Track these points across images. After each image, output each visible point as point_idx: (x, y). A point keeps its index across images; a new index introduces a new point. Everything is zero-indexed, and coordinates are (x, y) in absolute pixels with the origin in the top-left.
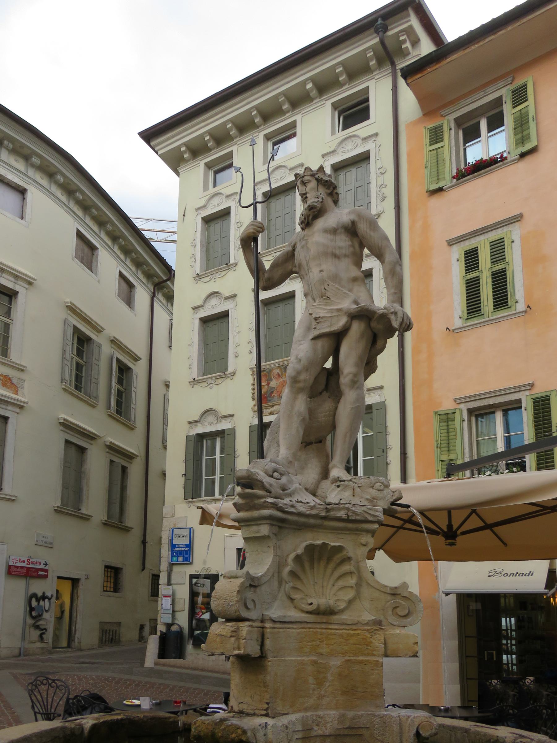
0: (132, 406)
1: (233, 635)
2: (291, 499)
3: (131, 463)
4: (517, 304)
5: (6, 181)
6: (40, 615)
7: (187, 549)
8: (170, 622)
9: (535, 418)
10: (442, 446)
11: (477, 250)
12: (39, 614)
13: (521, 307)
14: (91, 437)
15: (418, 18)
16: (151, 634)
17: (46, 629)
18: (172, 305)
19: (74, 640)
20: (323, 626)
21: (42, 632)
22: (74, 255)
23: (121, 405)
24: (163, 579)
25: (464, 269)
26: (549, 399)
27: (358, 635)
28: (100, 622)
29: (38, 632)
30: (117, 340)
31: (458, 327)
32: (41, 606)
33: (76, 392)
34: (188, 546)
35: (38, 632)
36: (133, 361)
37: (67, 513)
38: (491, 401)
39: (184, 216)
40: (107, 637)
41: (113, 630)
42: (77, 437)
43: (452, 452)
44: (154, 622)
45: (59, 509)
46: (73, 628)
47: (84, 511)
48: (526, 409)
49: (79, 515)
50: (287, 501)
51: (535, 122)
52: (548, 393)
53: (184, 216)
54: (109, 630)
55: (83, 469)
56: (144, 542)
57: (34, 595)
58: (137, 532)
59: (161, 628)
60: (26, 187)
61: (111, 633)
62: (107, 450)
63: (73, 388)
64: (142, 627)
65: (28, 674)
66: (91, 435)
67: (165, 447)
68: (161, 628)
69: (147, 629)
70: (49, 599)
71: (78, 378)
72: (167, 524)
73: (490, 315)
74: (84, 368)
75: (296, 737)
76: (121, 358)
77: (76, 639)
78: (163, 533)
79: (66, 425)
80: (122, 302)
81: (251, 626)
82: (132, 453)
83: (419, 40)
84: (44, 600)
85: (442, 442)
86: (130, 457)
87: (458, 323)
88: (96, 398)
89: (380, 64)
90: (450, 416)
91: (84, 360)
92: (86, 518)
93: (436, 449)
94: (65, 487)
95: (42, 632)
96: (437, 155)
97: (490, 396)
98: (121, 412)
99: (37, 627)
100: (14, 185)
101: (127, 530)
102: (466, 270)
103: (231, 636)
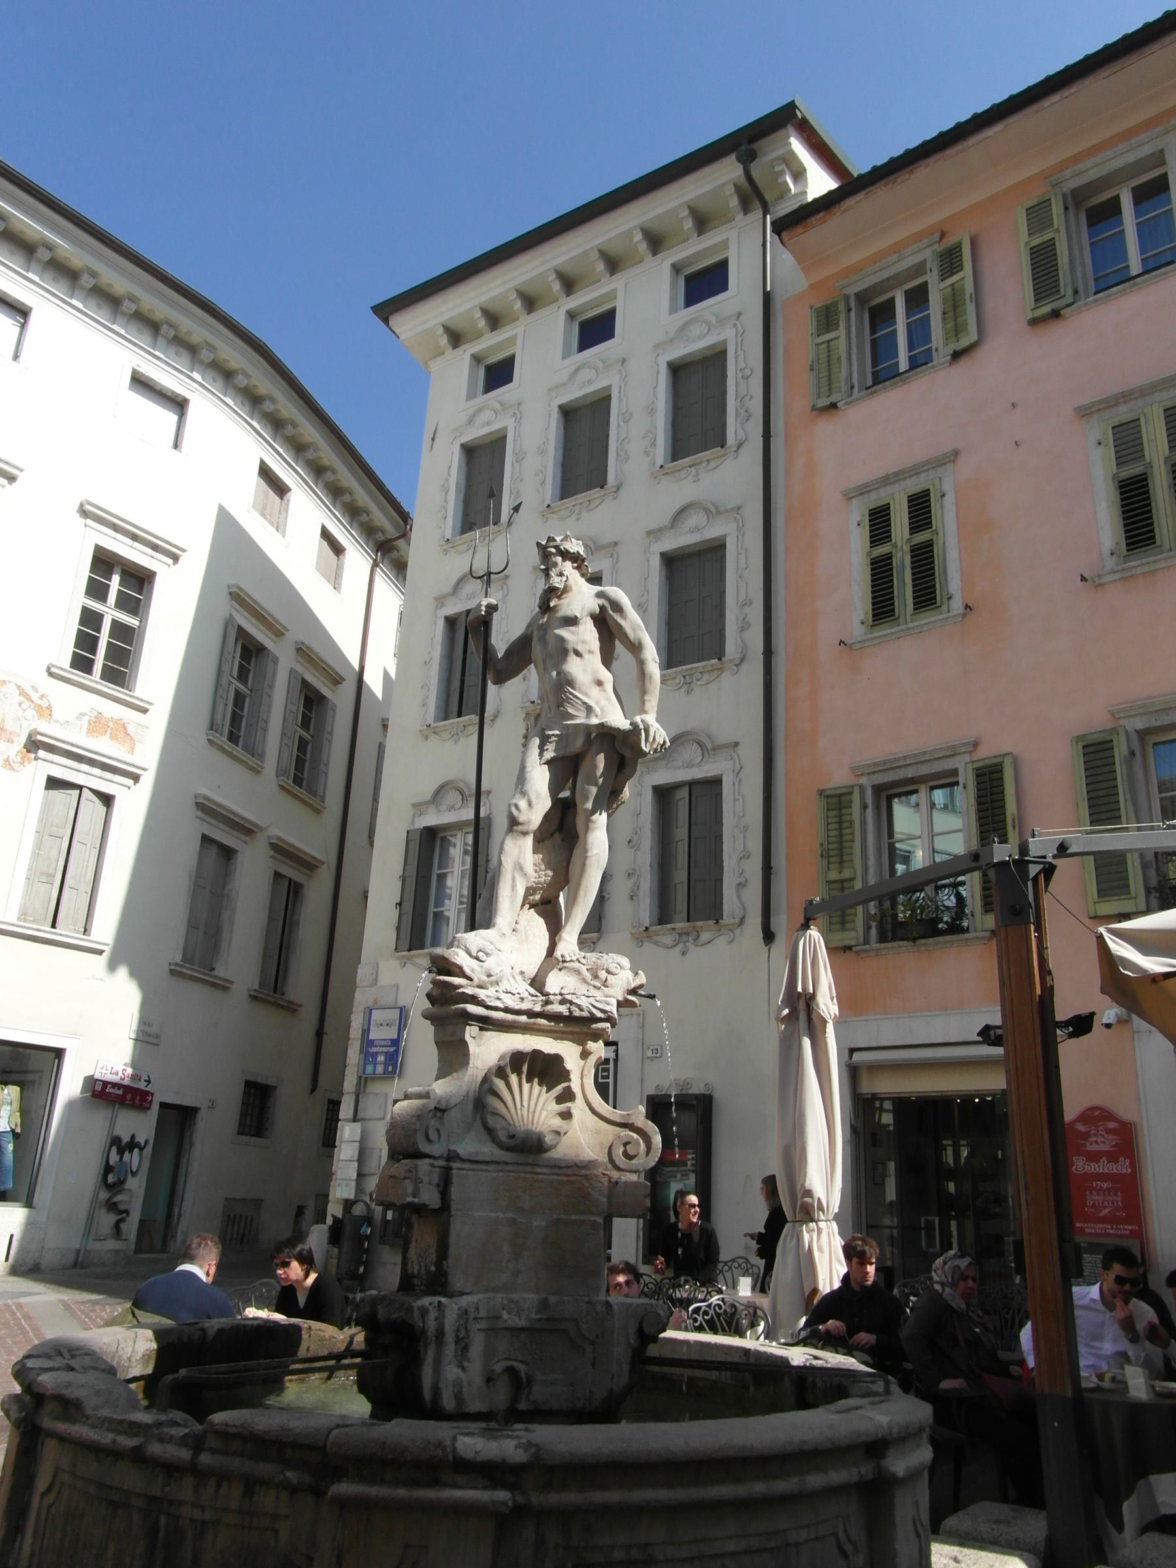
0: (322, 767)
1: (407, 1175)
2: (498, 988)
3: (310, 877)
4: (952, 601)
5: (158, 388)
6: (121, 1182)
7: (392, 1049)
8: (352, 1197)
9: (979, 804)
10: (832, 853)
11: (889, 509)
12: (119, 1179)
13: (957, 605)
14: (246, 829)
15: (802, 137)
16: (317, 1223)
17: (127, 1212)
18: (405, 578)
19: (174, 1237)
20: (528, 1169)
21: (120, 1217)
22: (251, 504)
23: (306, 747)
24: (346, 1111)
25: (868, 540)
26: (1001, 771)
27: (572, 1182)
28: (226, 1199)
29: (113, 1218)
30: (308, 648)
31: (859, 639)
32: (125, 1164)
33: (229, 746)
34: (396, 1043)
35: (113, 1218)
36: (329, 685)
37: (191, 976)
38: (910, 773)
39: (433, 439)
40: (236, 1230)
41: (247, 1217)
42: (223, 831)
43: (845, 865)
44: (323, 1198)
45: (178, 969)
46: (176, 1210)
47: (220, 971)
48: (965, 787)
49: (211, 980)
50: (491, 992)
51: (974, 303)
52: (999, 760)
53: (433, 439)
54: (241, 1217)
55: (226, 892)
56: (320, 1034)
57: (116, 1141)
58: (309, 1014)
59: (334, 1210)
60: (187, 397)
61: (243, 1223)
62: (272, 853)
63: (225, 739)
64: (300, 1211)
65: (89, 1301)
66: (246, 825)
67: (372, 844)
68: (334, 1210)
69: (309, 1214)
70: (141, 1149)
71: (236, 719)
72: (362, 998)
73: (909, 619)
74: (247, 701)
75: (478, 1326)
76: (310, 678)
77: (179, 1233)
78: (353, 1017)
79: (206, 808)
80: (322, 578)
81: (432, 1165)
82: (313, 858)
83: (805, 170)
84: (131, 1151)
85: (831, 846)
86: (309, 865)
87: (857, 631)
88: (261, 756)
89: (746, 207)
90: (844, 798)
91: (249, 686)
92: (222, 986)
93: (820, 859)
94: (192, 925)
95: (120, 1217)
96: (829, 351)
97: (908, 763)
98: (302, 780)
99: (112, 1206)
100: (169, 394)
101: (291, 1009)
102: (871, 543)
103: (405, 1178)
